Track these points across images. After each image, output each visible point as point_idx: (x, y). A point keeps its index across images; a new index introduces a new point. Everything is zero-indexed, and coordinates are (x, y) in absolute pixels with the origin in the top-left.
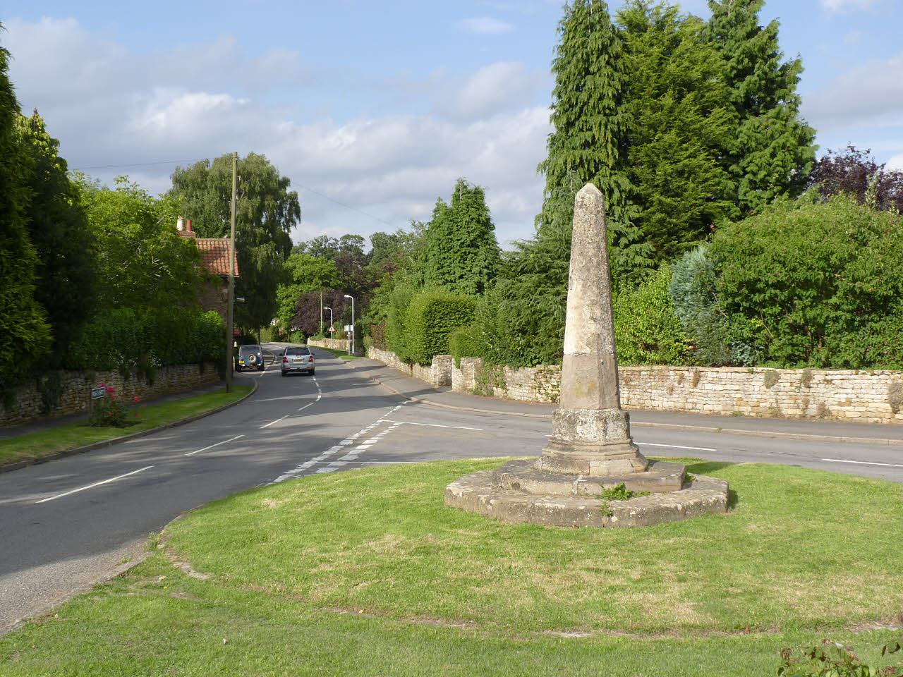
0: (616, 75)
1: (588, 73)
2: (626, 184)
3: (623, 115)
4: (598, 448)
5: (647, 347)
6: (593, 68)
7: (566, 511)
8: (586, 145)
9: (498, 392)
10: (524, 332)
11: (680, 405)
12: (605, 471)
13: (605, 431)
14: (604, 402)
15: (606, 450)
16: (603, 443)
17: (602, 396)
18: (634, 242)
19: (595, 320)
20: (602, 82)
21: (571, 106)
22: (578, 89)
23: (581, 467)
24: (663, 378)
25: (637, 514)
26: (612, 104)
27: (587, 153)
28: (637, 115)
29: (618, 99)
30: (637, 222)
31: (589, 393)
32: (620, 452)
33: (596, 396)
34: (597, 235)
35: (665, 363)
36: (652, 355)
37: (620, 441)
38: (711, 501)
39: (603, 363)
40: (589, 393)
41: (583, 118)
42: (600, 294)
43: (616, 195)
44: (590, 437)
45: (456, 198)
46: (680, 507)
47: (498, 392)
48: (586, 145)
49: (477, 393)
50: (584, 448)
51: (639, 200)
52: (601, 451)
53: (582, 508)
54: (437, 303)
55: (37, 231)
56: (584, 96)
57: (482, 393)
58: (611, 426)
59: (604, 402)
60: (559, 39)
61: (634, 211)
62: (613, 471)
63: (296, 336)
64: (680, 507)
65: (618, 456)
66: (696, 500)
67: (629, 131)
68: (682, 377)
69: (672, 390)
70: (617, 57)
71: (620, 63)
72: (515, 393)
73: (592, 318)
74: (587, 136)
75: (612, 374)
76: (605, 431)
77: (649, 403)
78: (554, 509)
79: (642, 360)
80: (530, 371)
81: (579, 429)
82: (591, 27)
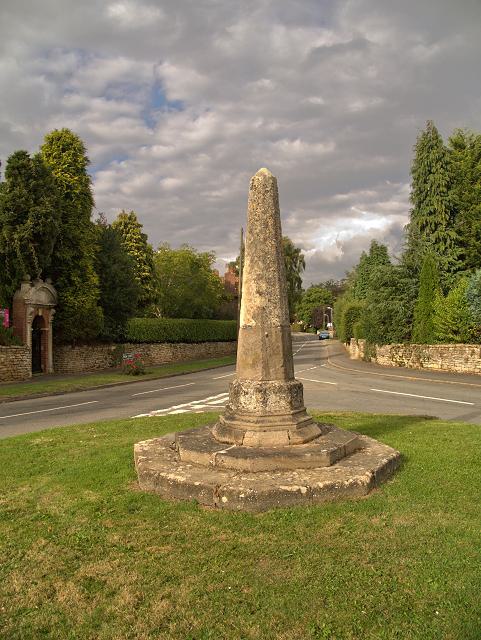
0: (447, 173)
1: (431, 173)
2: (454, 235)
3: (452, 195)
4: (255, 419)
5: (455, 332)
6: (433, 170)
7: (184, 484)
8: (431, 213)
9: (373, 359)
10: (384, 323)
11: (471, 369)
12: (256, 442)
13: (265, 402)
14: (267, 374)
15: (263, 422)
16: (260, 413)
17: (266, 367)
18: (459, 269)
19: (260, 294)
20: (439, 177)
21: (421, 192)
22: (425, 182)
23: (236, 437)
24: (462, 352)
25: (246, 498)
26: (445, 190)
27: (430, 219)
28: (460, 195)
29: (449, 188)
30: (461, 257)
31: (254, 365)
32: (279, 423)
33: (260, 368)
34: (264, 213)
35: (465, 342)
36: (458, 338)
37: (278, 413)
38: (346, 483)
39: (267, 336)
40: (254, 365)
41: (428, 198)
42: (267, 268)
43: (448, 242)
44: (251, 407)
45: (371, 251)
46: (304, 490)
47: (373, 359)
48: (431, 213)
49: (364, 359)
50: (242, 418)
51: (461, 244)
52: (257, 422)
53: (197, 484)
54: (353, 308)
55: (101, 269)
56: (428, 187)
57: (367, 360)
58: (272, 398)
59: (267, 374)
60: (414, 155)
61: (460, 251)
62: (264, 442)
63: (311, 330)
64: (304, 490)
65: (274, 428)
66: (327, 482)
67: (456, 205)
68: (473, 352)
69: (467, 360)
70: (447, 164)
71: (448, 167)
72: (381, 360)
73: (258, 292)
74: (431, 209)
75: (278, 347)
76: (265, 402)
77: (453, 368)
78: (174, 481)
79: (450, 341)
80: (388, 347)
81: (242, 399)
82: (432, 147)
